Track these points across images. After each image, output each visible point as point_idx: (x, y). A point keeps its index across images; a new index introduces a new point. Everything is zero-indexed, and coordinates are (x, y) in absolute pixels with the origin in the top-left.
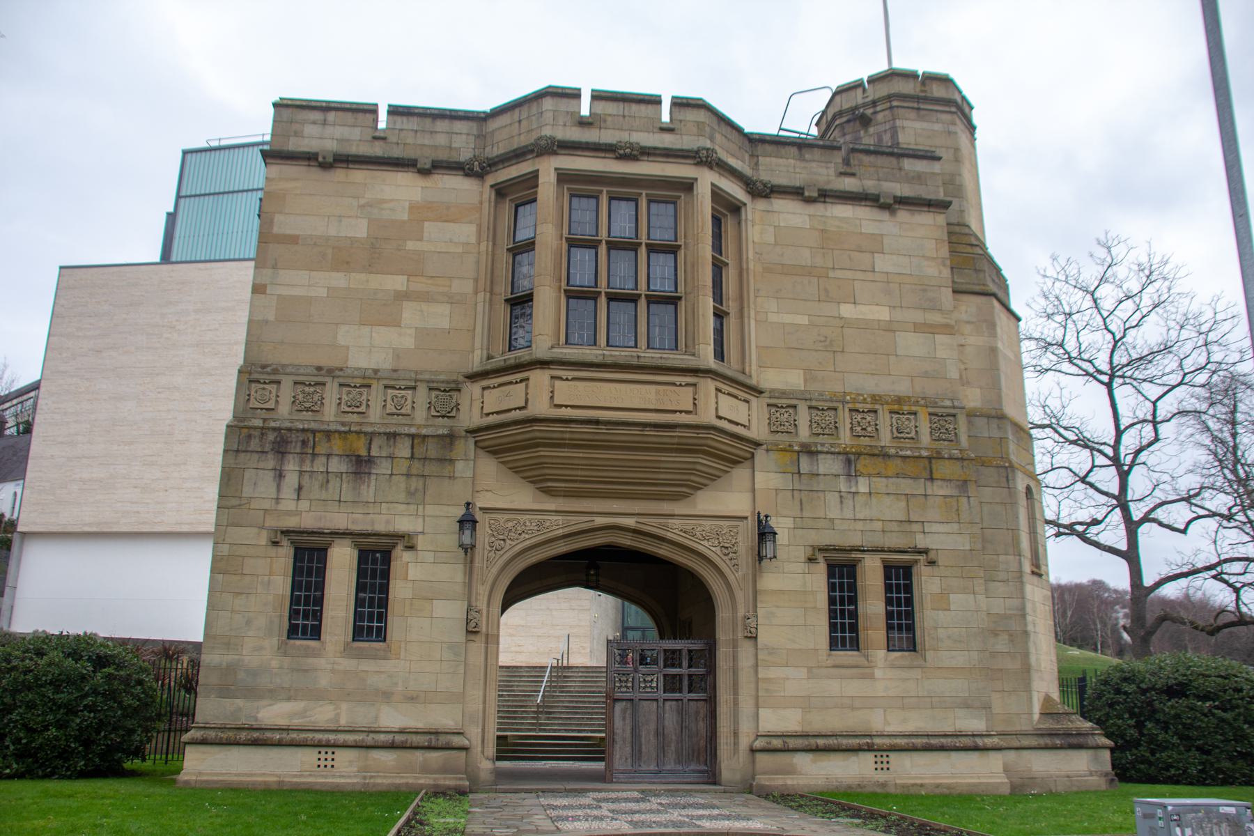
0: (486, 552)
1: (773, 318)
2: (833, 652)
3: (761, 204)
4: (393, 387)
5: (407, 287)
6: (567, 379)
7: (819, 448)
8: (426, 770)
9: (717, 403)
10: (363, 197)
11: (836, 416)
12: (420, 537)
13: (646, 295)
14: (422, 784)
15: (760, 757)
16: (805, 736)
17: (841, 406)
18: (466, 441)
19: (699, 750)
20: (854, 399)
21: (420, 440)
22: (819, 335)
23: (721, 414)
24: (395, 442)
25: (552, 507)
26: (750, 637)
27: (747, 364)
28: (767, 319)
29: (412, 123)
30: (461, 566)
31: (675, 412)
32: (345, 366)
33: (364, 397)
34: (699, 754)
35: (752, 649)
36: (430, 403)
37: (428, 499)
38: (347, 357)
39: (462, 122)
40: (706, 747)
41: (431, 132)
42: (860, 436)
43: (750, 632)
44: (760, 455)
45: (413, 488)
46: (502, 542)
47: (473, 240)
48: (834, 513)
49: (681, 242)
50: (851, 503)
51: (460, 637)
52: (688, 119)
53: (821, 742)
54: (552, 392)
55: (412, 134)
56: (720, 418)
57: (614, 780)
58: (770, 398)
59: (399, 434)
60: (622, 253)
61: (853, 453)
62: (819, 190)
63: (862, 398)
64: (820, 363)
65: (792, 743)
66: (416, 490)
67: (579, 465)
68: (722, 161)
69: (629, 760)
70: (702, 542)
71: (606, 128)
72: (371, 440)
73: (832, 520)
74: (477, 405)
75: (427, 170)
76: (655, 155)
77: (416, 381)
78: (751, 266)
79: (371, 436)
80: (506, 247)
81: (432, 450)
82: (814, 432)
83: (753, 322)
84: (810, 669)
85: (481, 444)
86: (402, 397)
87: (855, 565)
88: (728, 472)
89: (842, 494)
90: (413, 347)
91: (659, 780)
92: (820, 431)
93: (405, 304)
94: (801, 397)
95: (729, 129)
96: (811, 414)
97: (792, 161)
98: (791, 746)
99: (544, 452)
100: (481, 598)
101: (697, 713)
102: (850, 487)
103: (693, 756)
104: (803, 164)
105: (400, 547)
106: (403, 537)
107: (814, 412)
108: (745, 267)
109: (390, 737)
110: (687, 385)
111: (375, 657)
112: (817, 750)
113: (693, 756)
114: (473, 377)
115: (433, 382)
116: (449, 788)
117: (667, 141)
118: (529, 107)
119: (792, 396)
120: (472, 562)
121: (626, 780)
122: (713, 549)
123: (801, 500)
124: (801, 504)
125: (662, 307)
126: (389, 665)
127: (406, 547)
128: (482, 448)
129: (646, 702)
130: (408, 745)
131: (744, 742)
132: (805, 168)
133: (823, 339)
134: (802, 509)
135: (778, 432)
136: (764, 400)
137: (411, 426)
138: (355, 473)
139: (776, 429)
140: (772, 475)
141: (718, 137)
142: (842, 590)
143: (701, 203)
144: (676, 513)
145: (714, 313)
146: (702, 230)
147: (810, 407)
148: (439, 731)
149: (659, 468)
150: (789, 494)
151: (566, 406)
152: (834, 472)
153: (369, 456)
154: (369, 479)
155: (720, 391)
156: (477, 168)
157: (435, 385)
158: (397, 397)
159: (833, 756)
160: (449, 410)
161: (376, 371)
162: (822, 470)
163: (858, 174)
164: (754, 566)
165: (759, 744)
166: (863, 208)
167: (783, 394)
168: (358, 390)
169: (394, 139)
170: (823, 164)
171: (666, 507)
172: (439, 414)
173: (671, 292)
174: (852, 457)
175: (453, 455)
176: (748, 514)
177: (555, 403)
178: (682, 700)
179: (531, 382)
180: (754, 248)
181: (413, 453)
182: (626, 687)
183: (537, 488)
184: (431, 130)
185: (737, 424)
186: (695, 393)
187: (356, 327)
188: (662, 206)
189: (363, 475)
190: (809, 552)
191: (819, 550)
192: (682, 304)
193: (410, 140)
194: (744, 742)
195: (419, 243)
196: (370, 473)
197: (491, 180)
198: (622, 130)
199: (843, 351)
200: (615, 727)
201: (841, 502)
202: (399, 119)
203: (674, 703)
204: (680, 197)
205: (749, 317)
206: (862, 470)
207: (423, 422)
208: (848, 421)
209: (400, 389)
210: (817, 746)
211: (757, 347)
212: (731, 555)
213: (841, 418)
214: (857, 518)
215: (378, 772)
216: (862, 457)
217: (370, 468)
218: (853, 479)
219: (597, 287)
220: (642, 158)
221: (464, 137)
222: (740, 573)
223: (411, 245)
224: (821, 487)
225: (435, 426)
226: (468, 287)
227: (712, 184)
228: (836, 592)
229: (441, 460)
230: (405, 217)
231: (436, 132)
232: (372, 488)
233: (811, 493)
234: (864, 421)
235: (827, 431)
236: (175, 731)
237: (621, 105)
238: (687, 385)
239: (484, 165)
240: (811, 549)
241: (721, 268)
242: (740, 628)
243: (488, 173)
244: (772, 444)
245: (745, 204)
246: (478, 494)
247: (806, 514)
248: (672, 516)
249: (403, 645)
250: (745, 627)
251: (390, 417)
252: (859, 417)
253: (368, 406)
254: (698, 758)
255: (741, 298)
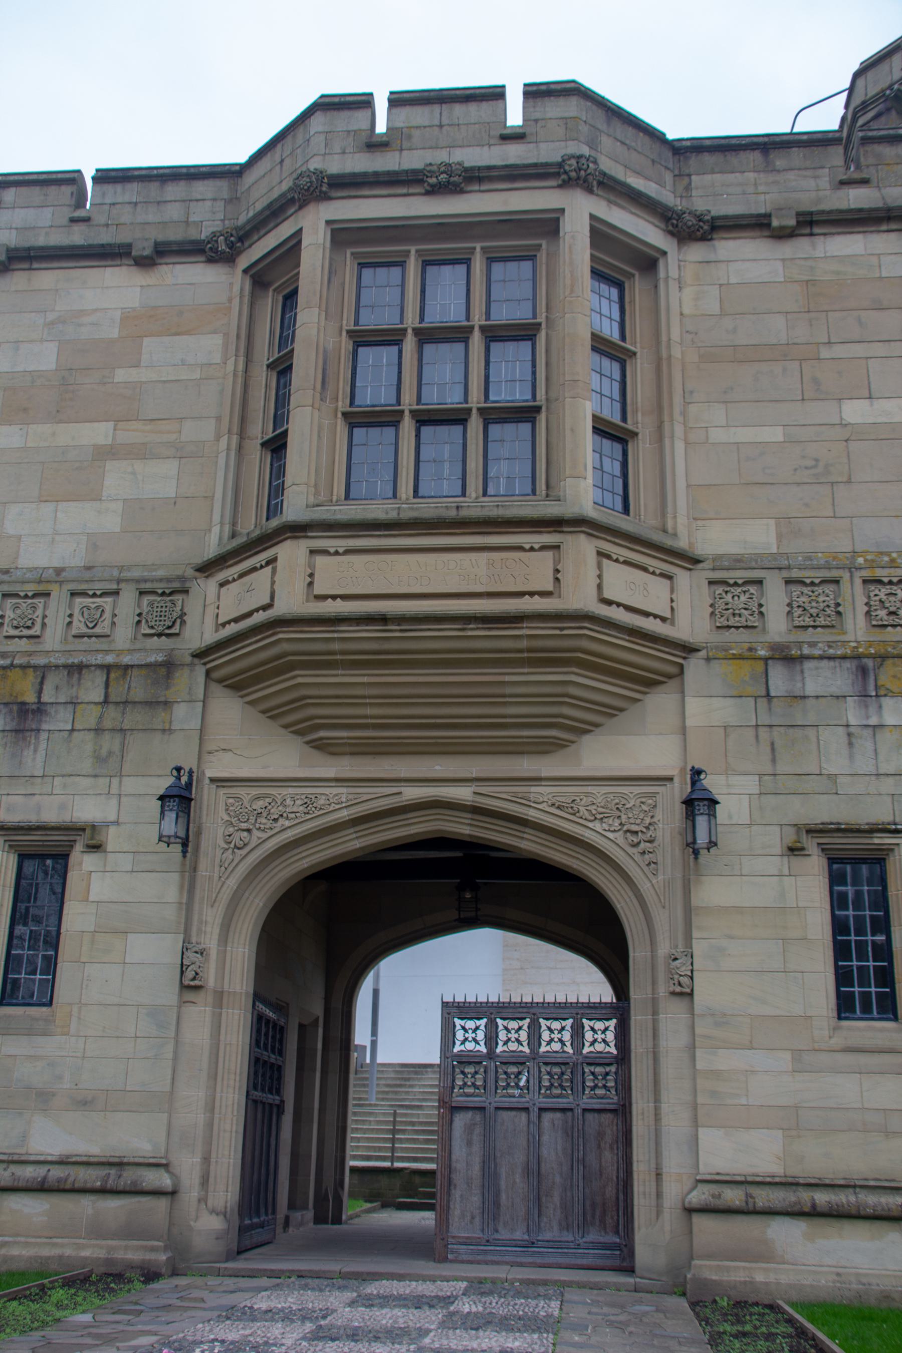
0: (219, 852)
1: (718, 435)
2: (845, 1023)
3: (696, 252)
4: (83, 594)
5: (114, 438)
6: (337, 553)
7: (806, 651)
8: (97, 1231)
9: (600, 577)
10: (53, 310)
11: (837, 594)
12: (112, 830)
13: (479, 409)
14: (86, 1258)
15: (699, 1221)
16: (792, 1184)
17: (846, 575)
18: (191, 671)
19: (604, 1204)
20: (873, 561)
21: (120, 672)
22: (804, 457)
23: (607, 595)
24: (79, 679)
25: (331, 773)
26: (681, 994)
27: (669, 516)
28: (707, 438)
29: (130, 192)
30: (176, 877)
31: (521, 594)
32: (13, 566)
33: (39, 612)
34: (604, 1213)
35: (685, 1016)
36: (140, 615)
37: (126, 768)
38: (18, 552)
39: (206, 182)
40: (617, 1198)
41: (159, 203)
42: (885, 626)
43: (680, 984)
44: (694, 667)
45: (104, 752)
46: (245, 834)
47: (217, 358)
48: (837, 763)
49: (541, 319)
50: (869, 745)
51: (169, 995)
52: (549, 115)
53: (822, 1198)
54: (311, 575)
55: (128, 208)
56: (609, 603)
57: (449, 1256)
58: (714, 569)
59: (88, 666)
60: (444, 347)
61: (869, 656)
62: (798, 214)
63: (886, 559)
64: (807, 505)
65: (763, 1197)
66: (110, 753)
67: (364, 697)
68: (611, 178)
69: (477, 1220)
70: (590, 825)
71: (410, 149)
72: (43, 678)
73: (833, 778)
74: (211, 611)
75: (146, 257)
76: (491, 179)
77: (119, 581)
78: (676, 352)
79: (43, 672)
80: (266, 362)
81: (138, 689)
82: (796, 623)
83: (680, 446)
84: (797, 1054)
85: (216, 675)
86: (97, 608)
87: (884, 859)
88: (639, 700)
89: (852, 729)
90: (118, 530)
91: (530, 1260)
92: (808, 621)
93: (109, 465)
94: (774, 564)
95: (630, 131)
96: (789, 594)
97: (751, 176)
98: (760, 1204)
99: (303, 677)
100: (209, 929)
101: (600, 1135)
102: (868, 717)
103: (593, 1216)
104: (771, 177)
105: (79, 847)
106: (84, 830)
107: (796, 589)
108: (664, 355)
109: (41, 1171)
110: (544, 548)
111: (30, 1032)
112: (813, 1213)
113: (593, 1216)
114: (207, 568)
115: (146, 581)
116: (131, 1266)
117: (514, 154)
118: (294, 136)
119: (753, 564)
120: (195, 869)
121: (471, 1258)
122: (611, 835)
123: (772, 744)
124: (773, 749)
125: (509, 428)
126: (48, 1046)
127: (88, 846)
128: (220, 681)
129: (509, 1113)
130: (68, 1186)
131: (673, 1191)
132: (775, 182)
133: (810, 463)
134: (774, 760)
135: (729, 627)
136: (703, 574)
137: (107, 652)
138: (16, 731)
139: (726, 623)
140: (717, 702)
141: (606, 142)
142: (858, 905)
143: (570, 247)
144: (543, 775)
145: (594, 427)
146: (572, 291)
147: (788, 582)
148: (125, 1160)
149: (504, 696)
150: (751, 732)
151: (334, 597)
152: (835, 691)
153: (39, 702)
154: (37, 738)
155: (608, 557)
156: (222, 247)
157: (148, 586)
158: (89, 608)
159: (848, 1227)
160: (170, 624)
161: (59, 571)
162: (811, 688)
163: (874, 180)
164: (685, 866)
165: (698, 1196)
166: (885, 236)
167: (738, 562)
168: (30, 601)
169: (102, 220)
170: (808, 173)
171: (526, 766)
172: (153, 631)
173: (527, 401)
174: (870, 663)
175: (170, 695)
176: (674, 772)
177: (316, 592)
178: (571, 1110)
179: (280, 563)
180: (681, 323)
181: (107, 695)
182: (605, 1086)
183: (307, 743)
184: (159, 199)
185: (647, 614)
186: (557, 561)
187: (34, 506)
188: (512, 266)
189: (28, 734)
190: (790, 837)
191: (808, 832)
192: (542, 417)
193: (126, 218)
194: (673, 1191)
195: (133, 371)
196: (39, 730)
197: (244, 261)
198: (437, 148)
199: (849, 481)
200: (454, 1157)
201: (851, 744)
202: (109, 188)
203: (558, 1115)
204: (540, 245)
205: (672, 437)
206: (889, 685)
207: (127, 646)
208: (861, 600)
209: (94, 595)
210: (814, 1206)
211: (688, 486)
212: (643, 845)
213: (848, 597)
214: (881, 772)
215: (17, 1235)
216: (889, 662)
217: (40, 721)
218: (872, 702)
219: (400, 405)
220: (469, 188)
221: (209, 204)
222: (661, 877)
223: (121, 375)
224: (811, 719)
225: (145, 650)
226: (206, 431)
227: (592, 217)
228: (847, 909)
229: (151, 704)
230: (115, 333)
231: (165, 202)
232: (41, 753)
233: (791, 730)
234: (892, 599)
235: (821, 621)
236: (393, 1140)
237: (436, 108)
238: (544, 548)
239: (232, 239)
240: (792, 830)
241: (625, 361)
242: (661, 976)
243: (240, 253)
244: (717, 648)
245: (664, 253)
246: (211, 757)
247: (781, 768)
248: (537, 780)
249: (75, 1010)
250: (671, 974)
251: (77, 640)
252: (883, 592)
253: (44, 625)
254: (603, 1221)
255: (659, 408)
